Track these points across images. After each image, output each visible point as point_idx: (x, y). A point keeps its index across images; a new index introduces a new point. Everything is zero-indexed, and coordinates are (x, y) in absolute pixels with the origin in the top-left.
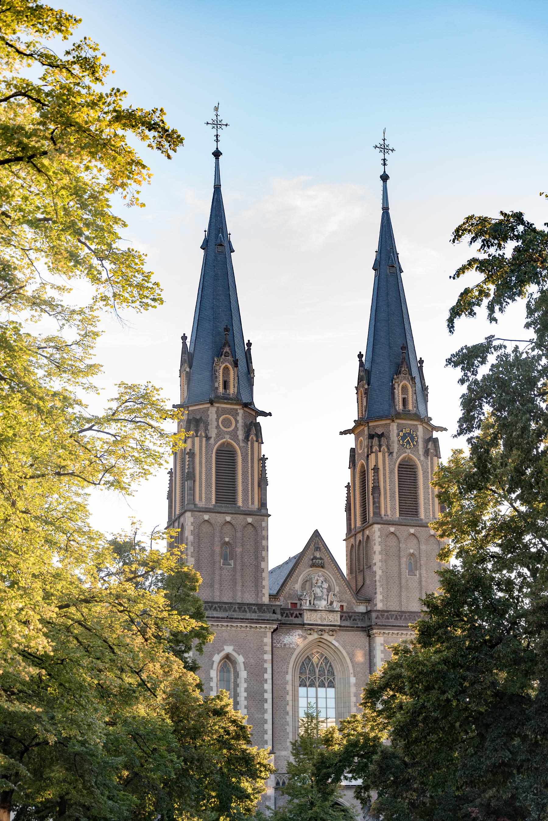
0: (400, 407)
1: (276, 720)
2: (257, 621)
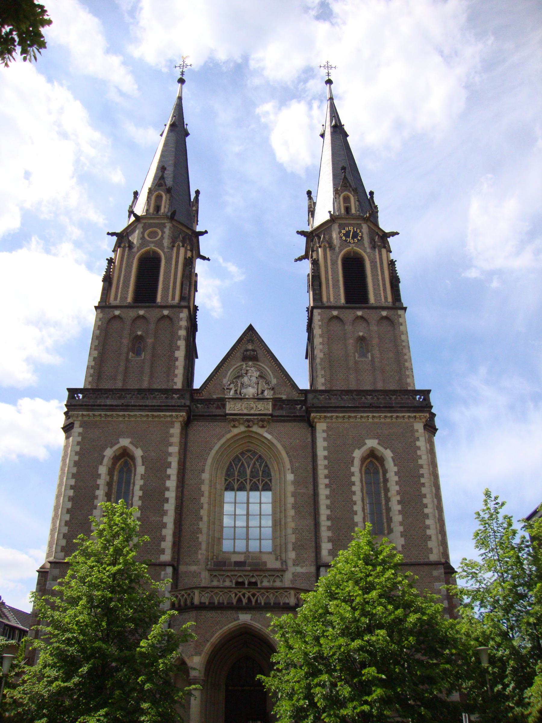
2: (159, 408)
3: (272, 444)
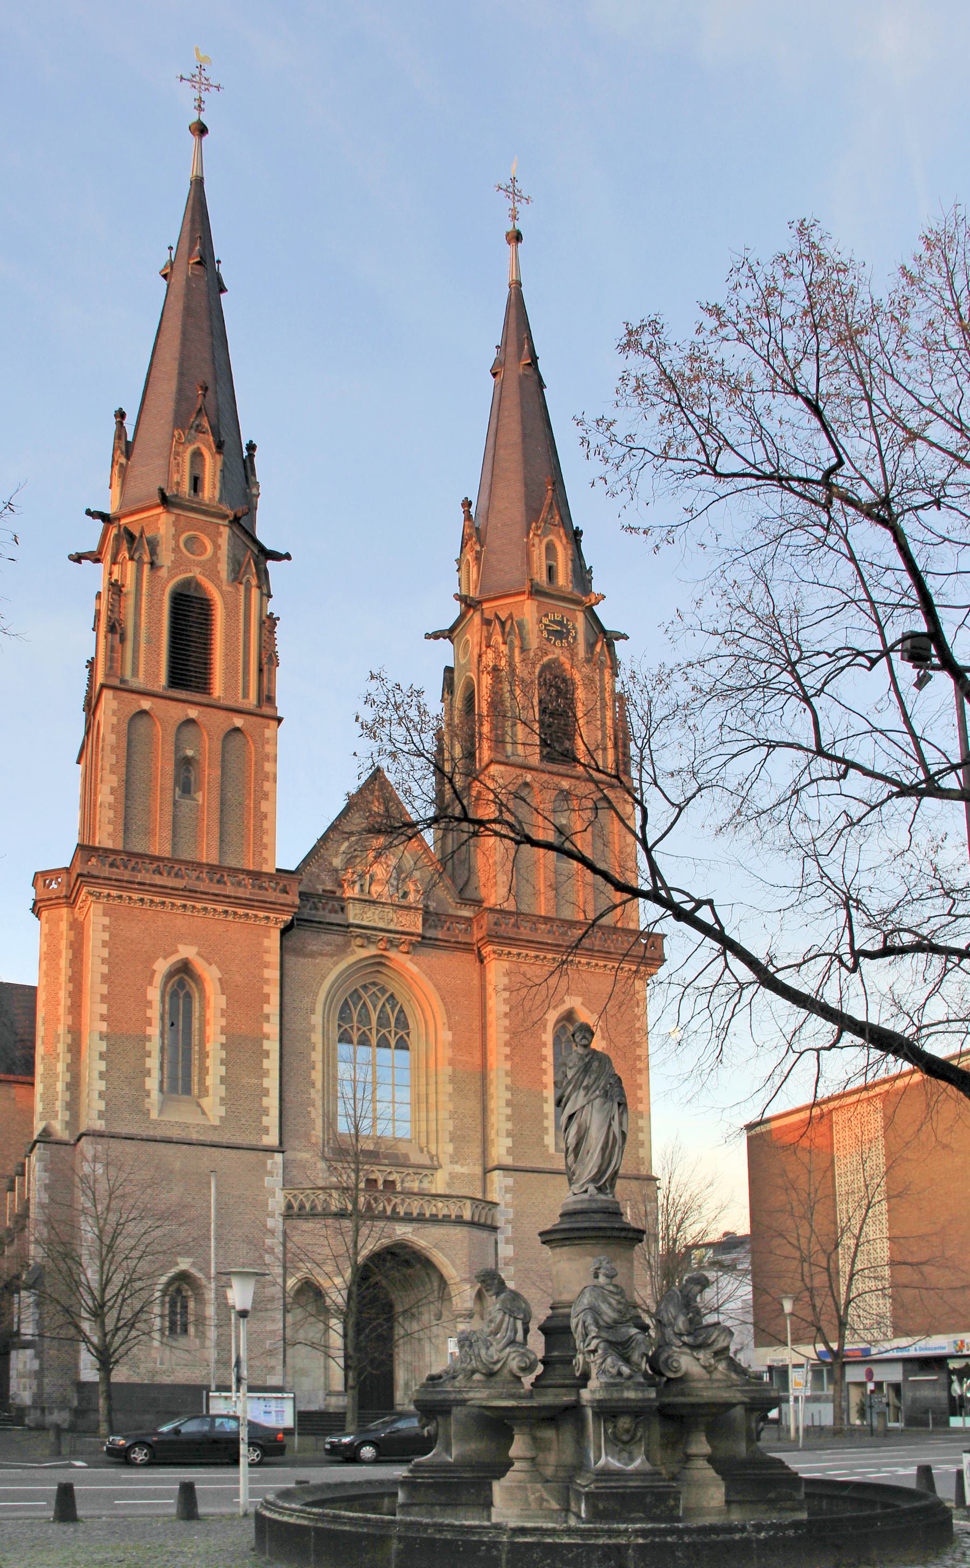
0: (541, 577)
1: (289, 1096)
2: (248, 903)
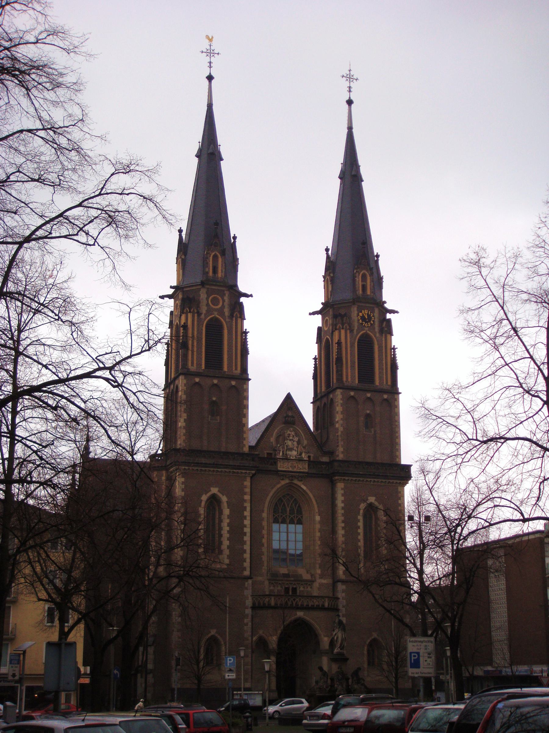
3: (307, 493)
